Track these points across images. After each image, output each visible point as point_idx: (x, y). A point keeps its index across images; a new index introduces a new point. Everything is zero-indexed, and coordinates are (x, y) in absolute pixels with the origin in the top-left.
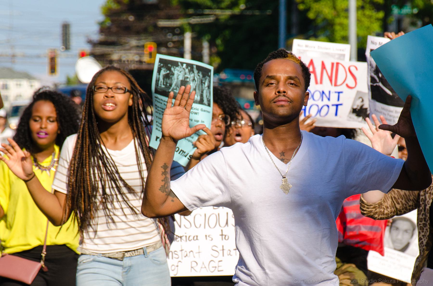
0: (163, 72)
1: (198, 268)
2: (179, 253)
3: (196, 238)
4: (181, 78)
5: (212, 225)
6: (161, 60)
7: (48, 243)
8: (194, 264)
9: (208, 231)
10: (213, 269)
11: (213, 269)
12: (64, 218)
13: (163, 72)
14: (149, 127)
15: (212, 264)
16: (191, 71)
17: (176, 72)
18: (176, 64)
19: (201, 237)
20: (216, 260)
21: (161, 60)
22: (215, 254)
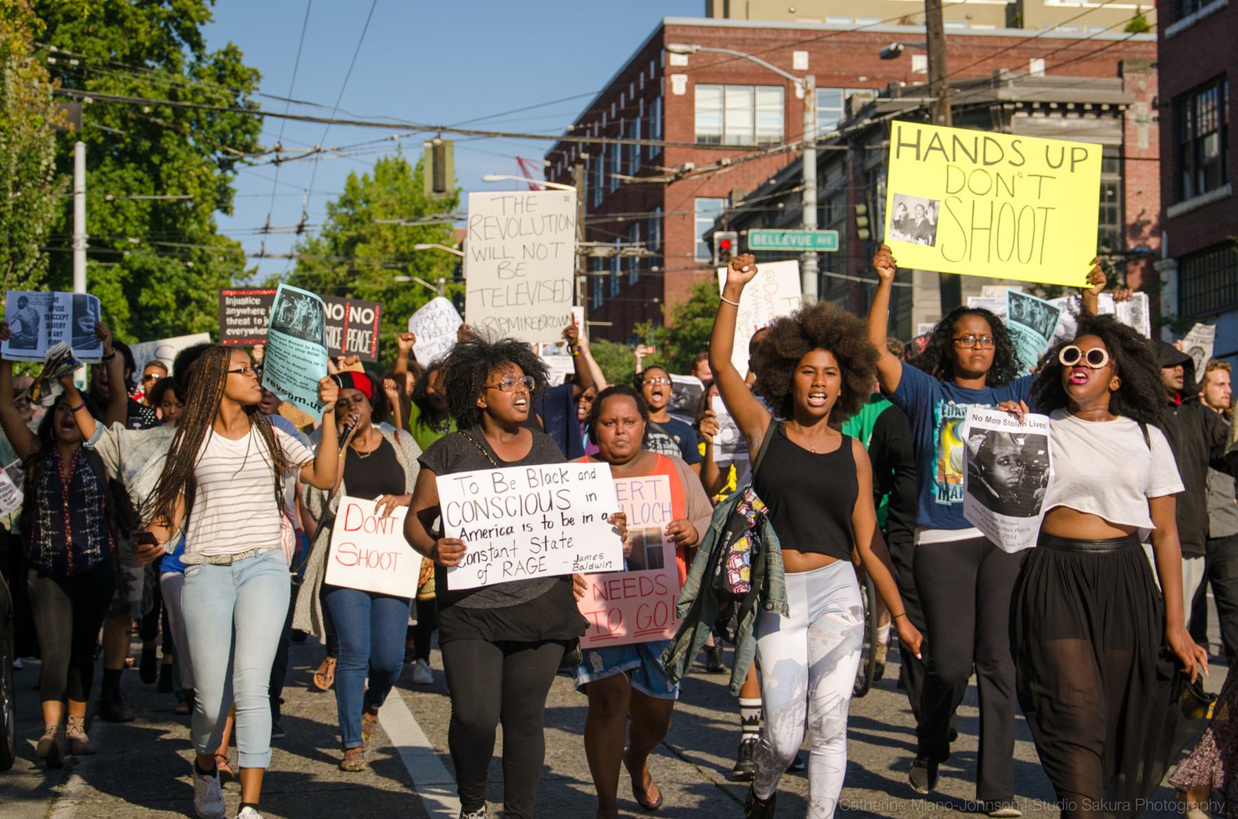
0: (284, 305)
1: (512, 571)
2: (488, 553)
3: (510, 531)
4: (304, 313)
5: (531, 510)
6: (284, 291)
7: (667, 277)
8: (508, 565)
9: (526, 519)
10: (531, 570)
11: (531, 570)
12: (284, 364)
13: (284, 305)
14: (351, 197)
15: (532, 562)
16: (314, 306)
17: (299, 306)
18: (300, 296)
19: (518, 529)
20: (537, 556)
21: (284, 291)
22: (536, 548)
